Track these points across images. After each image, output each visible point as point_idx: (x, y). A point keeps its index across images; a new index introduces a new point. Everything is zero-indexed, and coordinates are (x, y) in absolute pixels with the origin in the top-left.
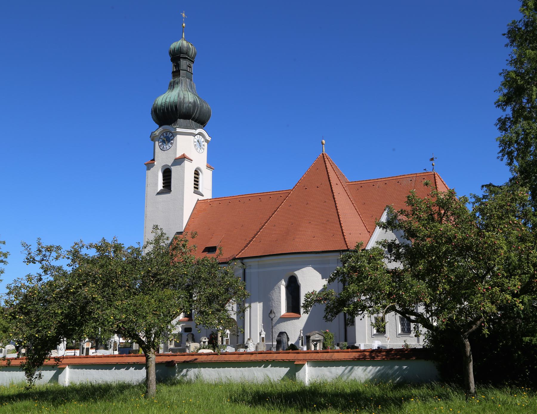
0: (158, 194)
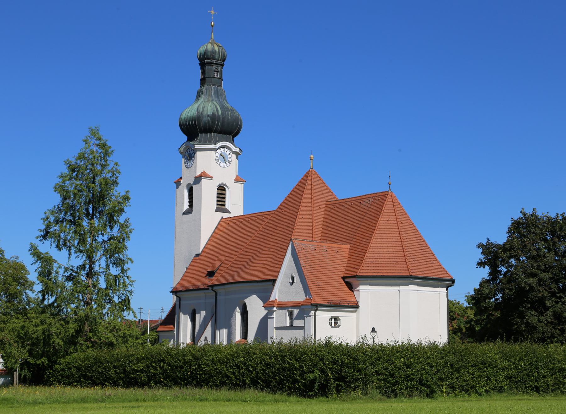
0: (184, 213)
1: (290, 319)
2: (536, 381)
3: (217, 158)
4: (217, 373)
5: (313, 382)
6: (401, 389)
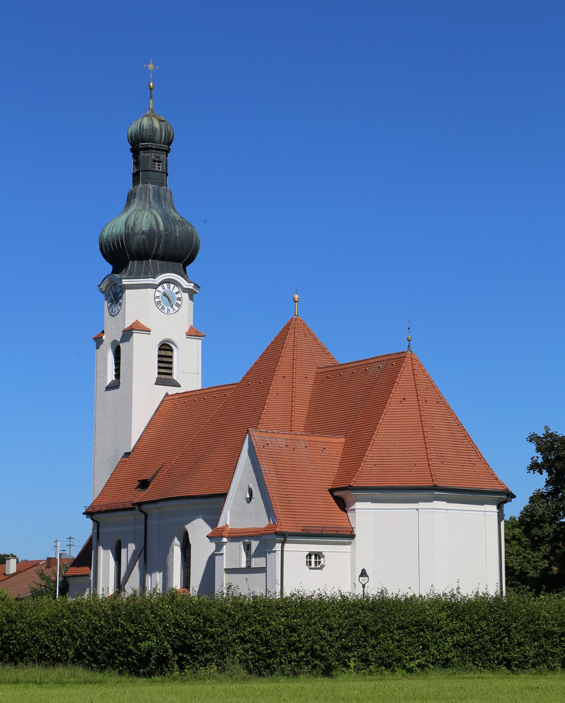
0: (108, 388)
1: (247, 557)
2: (506, 650)
3: (157, 300)
4: (35, 641)
5: (149, 652)
6: (281, 663)
